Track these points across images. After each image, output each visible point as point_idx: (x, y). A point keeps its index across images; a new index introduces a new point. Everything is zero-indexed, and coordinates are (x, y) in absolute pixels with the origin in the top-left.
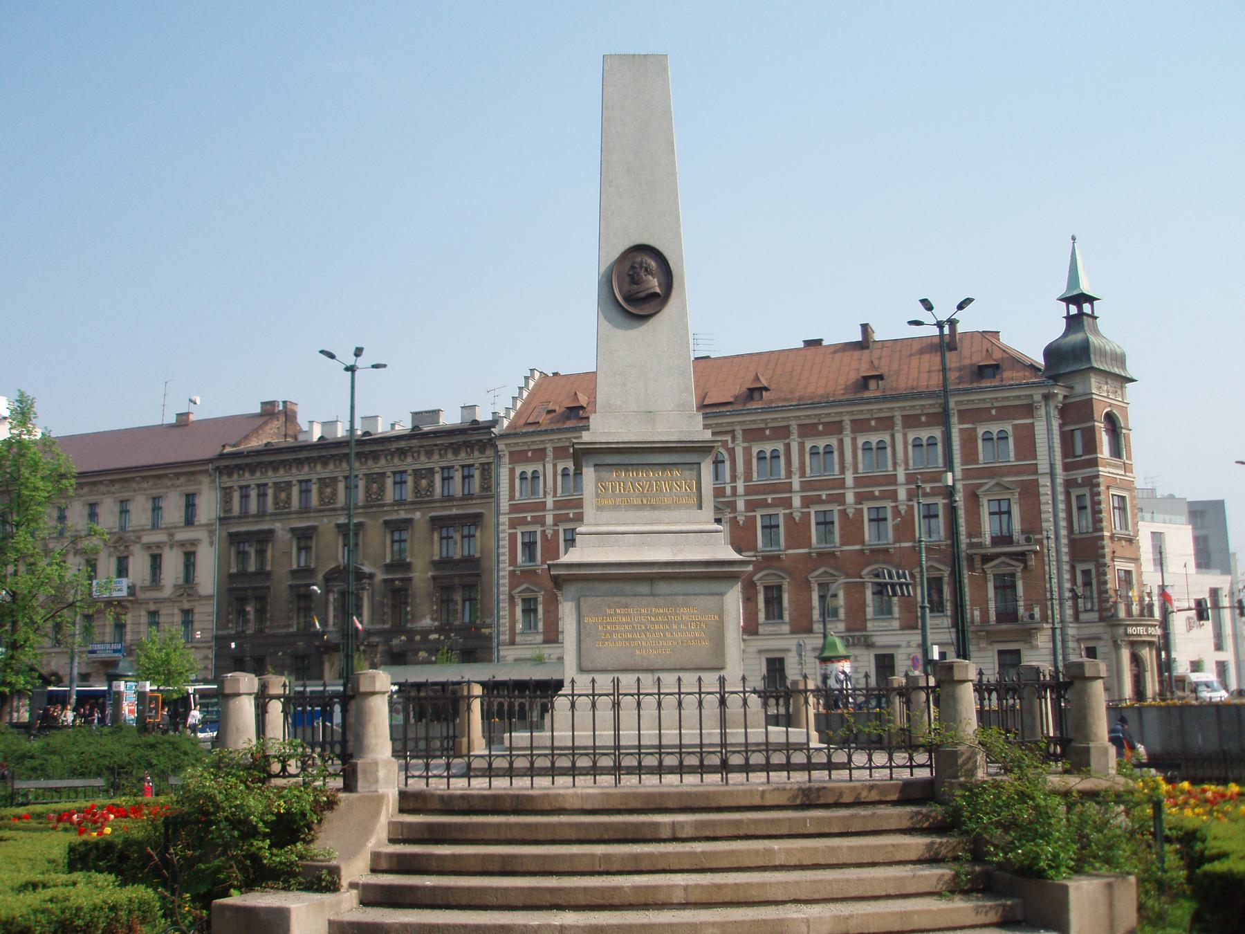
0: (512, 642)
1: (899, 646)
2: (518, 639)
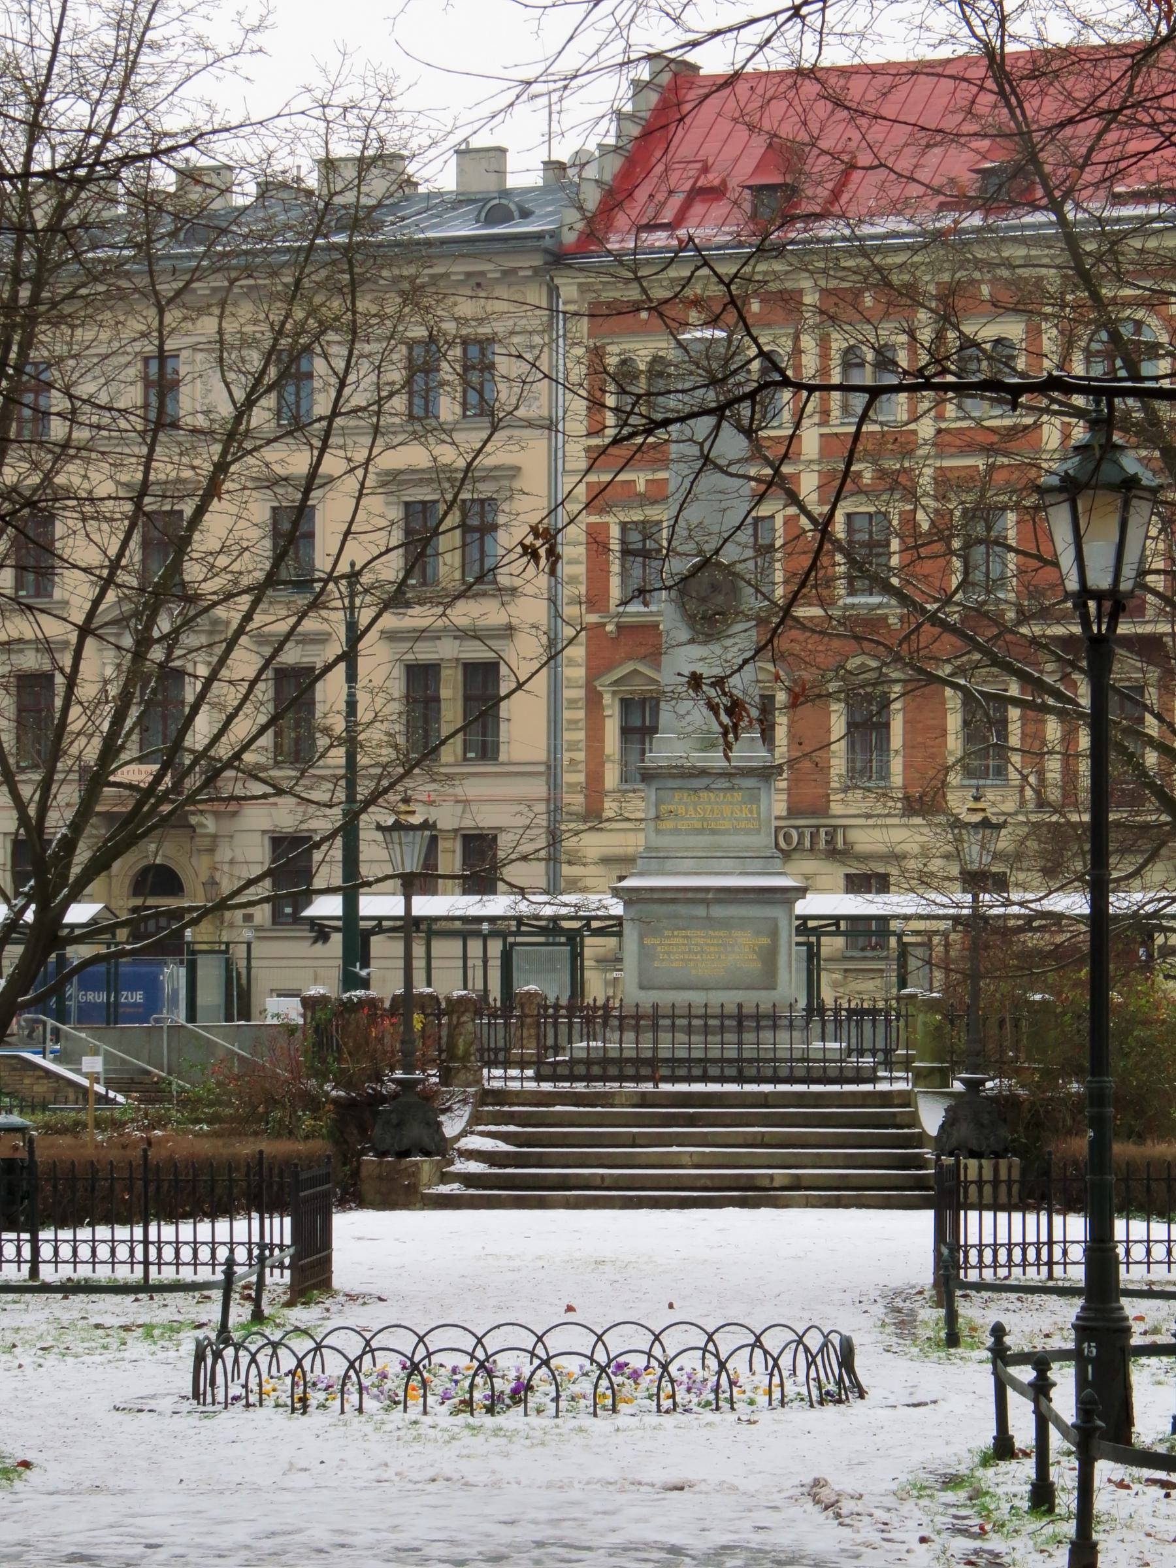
0: (593, 816)
1: (898, 857)
2: (610, 808)
